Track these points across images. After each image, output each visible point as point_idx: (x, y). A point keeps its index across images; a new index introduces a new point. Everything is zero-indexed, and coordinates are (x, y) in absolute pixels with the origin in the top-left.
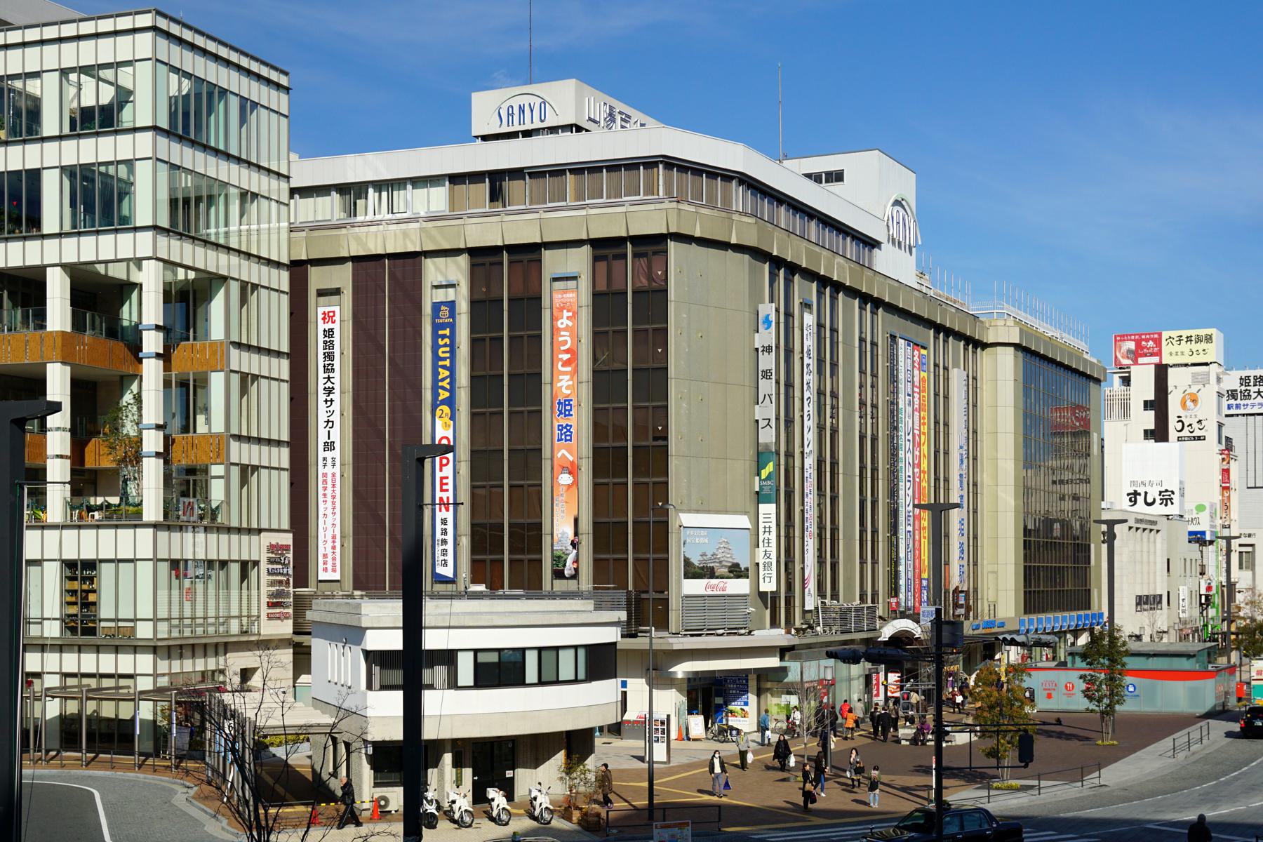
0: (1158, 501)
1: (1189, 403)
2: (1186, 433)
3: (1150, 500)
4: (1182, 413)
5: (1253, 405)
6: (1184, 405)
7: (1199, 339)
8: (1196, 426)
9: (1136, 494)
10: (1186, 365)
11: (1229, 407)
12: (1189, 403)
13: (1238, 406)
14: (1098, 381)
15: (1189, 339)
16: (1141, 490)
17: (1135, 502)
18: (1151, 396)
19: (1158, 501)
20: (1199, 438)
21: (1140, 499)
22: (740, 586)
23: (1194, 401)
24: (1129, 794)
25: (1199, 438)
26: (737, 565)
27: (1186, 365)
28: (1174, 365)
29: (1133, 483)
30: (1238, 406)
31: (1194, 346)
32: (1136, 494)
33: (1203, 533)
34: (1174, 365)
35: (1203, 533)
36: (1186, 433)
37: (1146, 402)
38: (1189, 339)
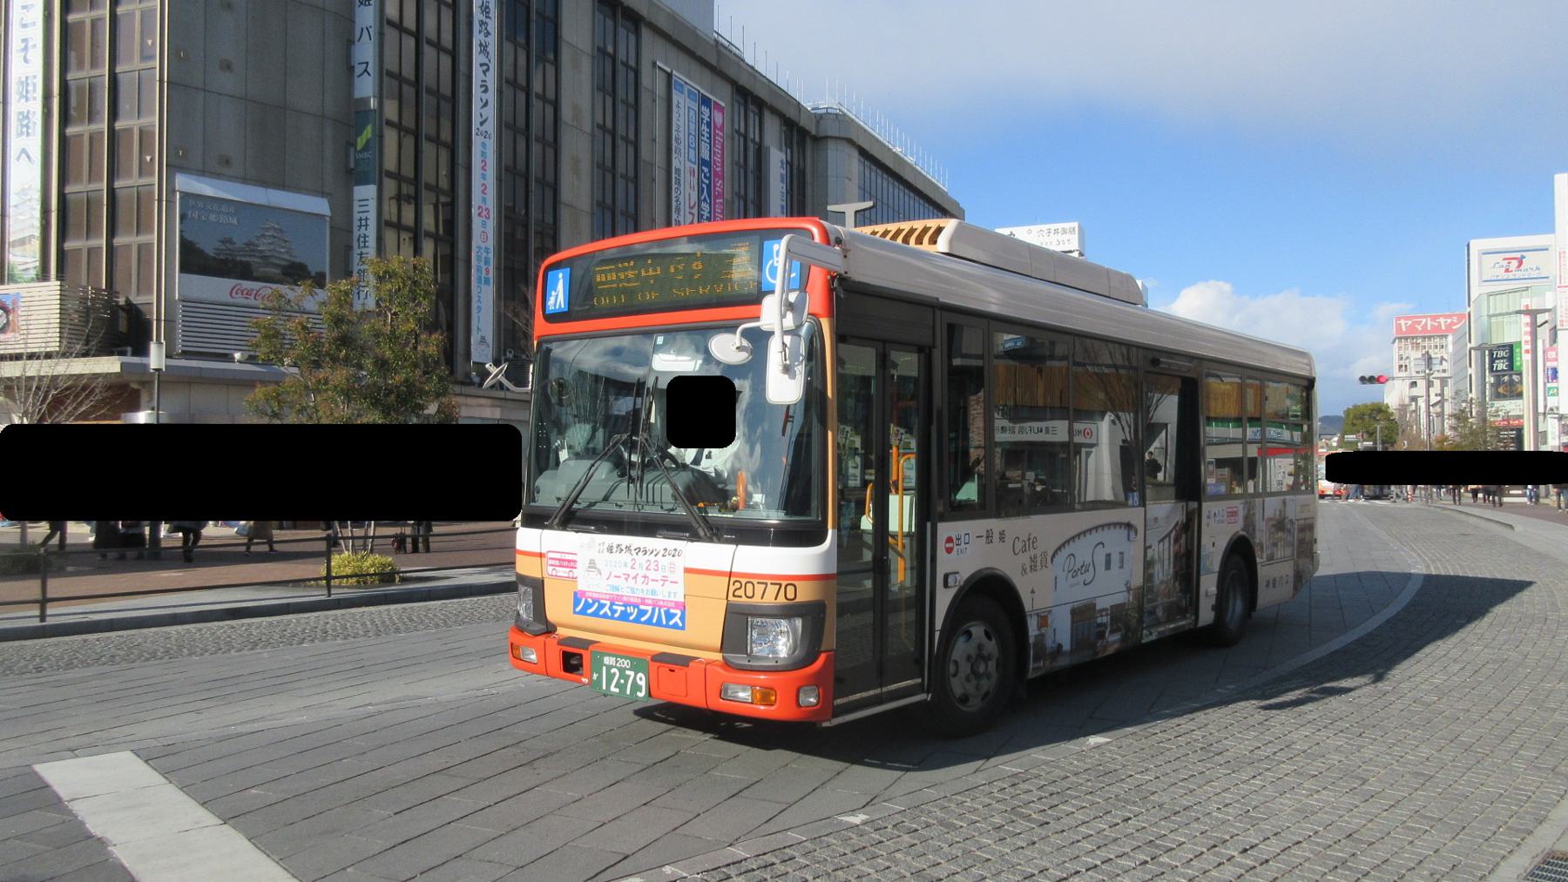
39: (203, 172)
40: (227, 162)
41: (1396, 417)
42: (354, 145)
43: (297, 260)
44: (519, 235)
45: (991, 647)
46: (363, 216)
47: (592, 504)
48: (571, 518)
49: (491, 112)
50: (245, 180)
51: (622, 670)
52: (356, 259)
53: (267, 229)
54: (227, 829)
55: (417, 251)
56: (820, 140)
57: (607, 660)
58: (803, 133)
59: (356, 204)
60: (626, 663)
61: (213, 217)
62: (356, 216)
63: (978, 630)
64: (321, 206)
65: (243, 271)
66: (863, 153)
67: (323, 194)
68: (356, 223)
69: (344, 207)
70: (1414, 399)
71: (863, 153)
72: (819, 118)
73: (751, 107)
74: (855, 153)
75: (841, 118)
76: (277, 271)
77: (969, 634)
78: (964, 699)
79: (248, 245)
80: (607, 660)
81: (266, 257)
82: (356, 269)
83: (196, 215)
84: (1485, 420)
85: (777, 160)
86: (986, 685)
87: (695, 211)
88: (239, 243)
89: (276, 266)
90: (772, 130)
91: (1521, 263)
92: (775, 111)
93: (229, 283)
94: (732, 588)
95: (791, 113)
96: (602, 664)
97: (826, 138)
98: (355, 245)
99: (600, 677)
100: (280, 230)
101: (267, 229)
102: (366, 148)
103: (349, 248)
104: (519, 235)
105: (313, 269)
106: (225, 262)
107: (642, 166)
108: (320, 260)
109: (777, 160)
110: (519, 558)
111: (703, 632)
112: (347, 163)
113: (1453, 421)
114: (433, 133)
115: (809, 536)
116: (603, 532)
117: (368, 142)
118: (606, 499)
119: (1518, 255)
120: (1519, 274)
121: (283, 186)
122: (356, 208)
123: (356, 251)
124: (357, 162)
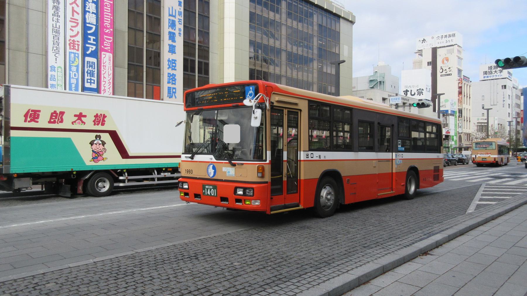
0: (416, 94)
1: (445, 61)
2: (444, 73)
3: (413, 93)
4: (442, 65)
5: (493, 76)
6: (443, 62)
7: (450, 36)
8: (448, 70)
9: (407, 91)
10: (444, 47)
11: (484, 77)
12: (445, 61)
13: (488, 77)
14: (352, 22)
15: (446, 36)
16: (409, 89)
17: (407, 95)
18: (430, 60)
19: (416, 94)
20: (449, 75)
21: (409, 93)
23: (447, 60)
24: (181, 203)
25: (449, 75)
27: (444, 47)
28: (440, 47)
29: (406, 87)
30: (488, 77)
31: (448, 39)
32: (407, 91)
33: (447, 111)
34: (440, 47)
35: (447, 111)
36: (444, 73)
37: (428, 63)
57: (207, 187)
60: (211, 187)
80: (207, 187)
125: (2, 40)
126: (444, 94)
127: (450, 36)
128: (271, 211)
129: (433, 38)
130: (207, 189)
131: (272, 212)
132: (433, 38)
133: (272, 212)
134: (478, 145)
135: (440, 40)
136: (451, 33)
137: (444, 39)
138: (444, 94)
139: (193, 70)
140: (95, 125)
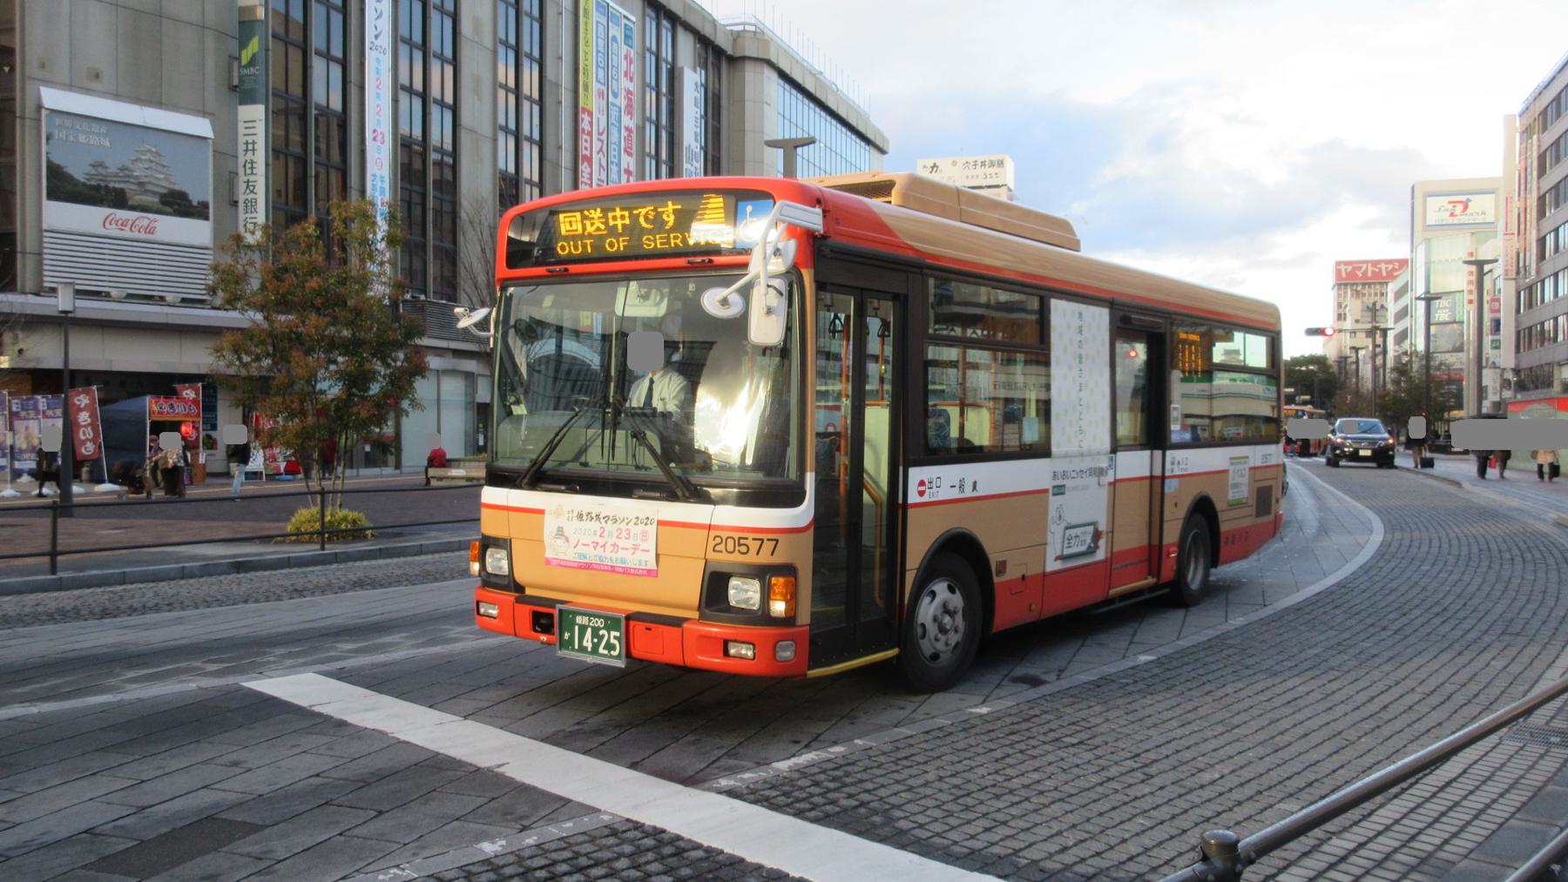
7: (992, 164)
15: (983, 164)
22: (197, 232)
26: (183, 196)
38: (983, 164)
39: (70, 87)
40: (97, 76)
41: (1335, 369)
42: (239, 59)
43: (177, 187)
44: (417, 165)
45: (957, 601)
46: (250, 139)
47: (562, 463)
48: (538, 477)
49: (385, 25)
50: (117, 96)
51: (595, 631)
52: (242, 187)
53: (143, 153)
54: (468, 722)
55: (975, 366)
56: (735, 61)
57: (579, 619)
58: (718, 52)
59: (241, 126)
60: (600, 623)
61: (82, 138)
62: (241, 140)
63: (941, 588)
64: (201, 126)
65: (118, 199)
66: (783, 75)
67: (204, 113)
68: (241, 147)
69: (227, 128)
70: (1356, 349)
71: (783, 75)
72: (737, 37)
73: (664, 22)
74: (774, 76)
75: (759, 35)
76: (156, 200)
77: (933, 594)
78: (935, 656)
79: (122, 169)
80: (579, 619)
81: (141, 184)
82: (241, 199)
83: (63, 135)
84: (1428, 367)
85: (692, 82)
86: (954, 639)
87: (604, 137)
88: (113, 169)
89: (155, 193)
90: (686, 44)
91: (1466, 207)
92: (689, 28)
93: (103, 212)
94: (711, 544)
95: (707, 31)
96: (573, 623)
97: (744, 58)
98: (241, 171)
99: (572, 637)
100: (158, 154)
101: (143, 153)
102: (252, 63)
103: (234, 174)
104: (417, 165)
105: (195, 198)
106: (97, 188)
107: (547, 88)
108: (201, 189)
109: (692, 82)
110: (485, 513)
111: (686, 589)
112: (230, 78)
113: (1395, 375)
114: (323, 48)
115: (788, 496)
116: (574, 491)
117: (254, 55)
118: (576, 458)
119: (1463, 198)
120: (1465, 219)
121: (158, 103)
122: (241, 131)
123: (242, 178)
124: (241, 78)
125: (4, 43)
126: (882, 151)
127: (992, 164)
128: (810, 668)
129: (954, 163)
130: (583, 629)
131: (814, 673)
132: (954, 163)
133: (814, 673)
134: (1042, 407)
135: (972, 172)
136: (995, 158)
137: (980, 171)
138: (882, 151)
139: (439, 213)
140: (818, 435)
